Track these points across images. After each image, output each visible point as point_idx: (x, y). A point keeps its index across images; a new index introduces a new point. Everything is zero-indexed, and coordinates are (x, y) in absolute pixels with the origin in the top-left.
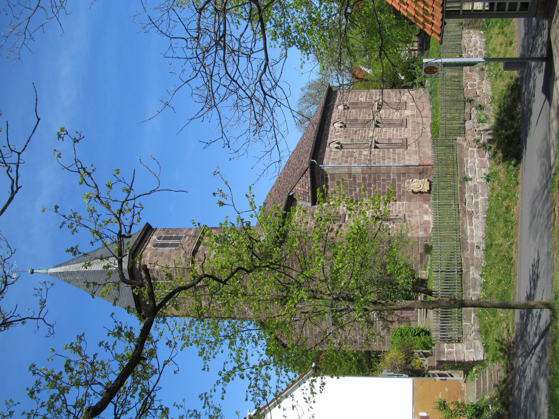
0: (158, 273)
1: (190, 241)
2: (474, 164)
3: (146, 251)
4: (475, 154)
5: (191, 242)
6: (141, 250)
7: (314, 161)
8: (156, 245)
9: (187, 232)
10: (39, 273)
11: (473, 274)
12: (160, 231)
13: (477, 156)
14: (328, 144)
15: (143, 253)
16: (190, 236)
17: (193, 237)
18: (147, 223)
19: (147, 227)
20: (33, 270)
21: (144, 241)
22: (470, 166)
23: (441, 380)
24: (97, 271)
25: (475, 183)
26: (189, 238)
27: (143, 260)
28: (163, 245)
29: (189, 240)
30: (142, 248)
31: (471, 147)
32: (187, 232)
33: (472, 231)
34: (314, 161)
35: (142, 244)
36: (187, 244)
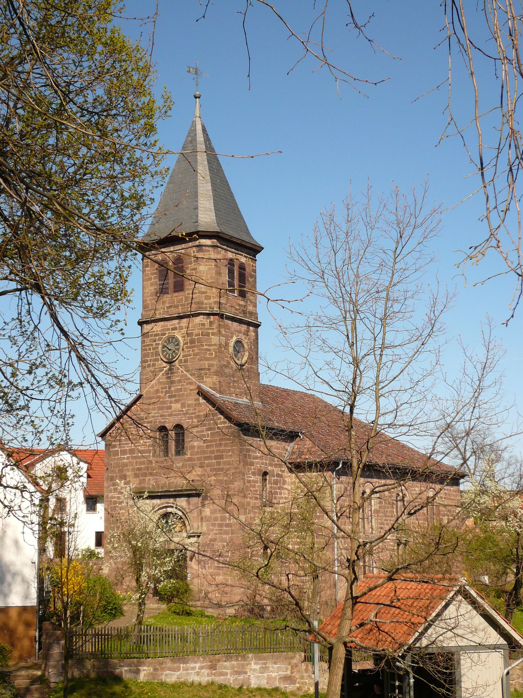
0: (195, 269)
1: (238, 307)
2: (271, 672)
3: (223, 252)
4: (283, 673)
5: (236, 309)
6: (224, 245)
7: (341, 466)
8: (231, 262)
9: (251, 302)
10: (196, 106)
11: (144, 670)
12: (253, 266)
13: (281, 675)
14: (369, 480)
15: (219, 249)
16: (245, 306)
17: (243, 311)
18: (263, 248)
19: (256, 248)
20: (199, 98)
21: (237, 247)
22: (269, 667)
23: (35, 637)
24: (197, 188)
25: (248, 673)
26: (242, 305)
27: (211, 249)
28: (231, 273)
29: (240, 305)
30: (227, 246)
31: (292, 667)
32: (251, 302)
33: (193, 668)
34: (341, 466)
35: (232, 245)
36: (234, 305)
